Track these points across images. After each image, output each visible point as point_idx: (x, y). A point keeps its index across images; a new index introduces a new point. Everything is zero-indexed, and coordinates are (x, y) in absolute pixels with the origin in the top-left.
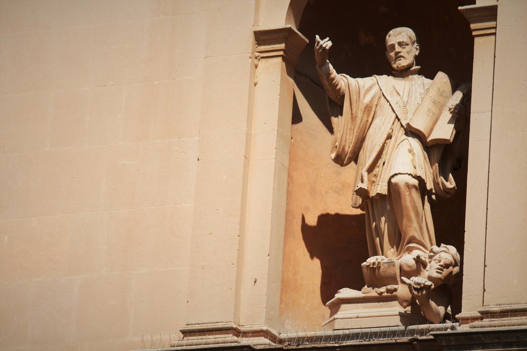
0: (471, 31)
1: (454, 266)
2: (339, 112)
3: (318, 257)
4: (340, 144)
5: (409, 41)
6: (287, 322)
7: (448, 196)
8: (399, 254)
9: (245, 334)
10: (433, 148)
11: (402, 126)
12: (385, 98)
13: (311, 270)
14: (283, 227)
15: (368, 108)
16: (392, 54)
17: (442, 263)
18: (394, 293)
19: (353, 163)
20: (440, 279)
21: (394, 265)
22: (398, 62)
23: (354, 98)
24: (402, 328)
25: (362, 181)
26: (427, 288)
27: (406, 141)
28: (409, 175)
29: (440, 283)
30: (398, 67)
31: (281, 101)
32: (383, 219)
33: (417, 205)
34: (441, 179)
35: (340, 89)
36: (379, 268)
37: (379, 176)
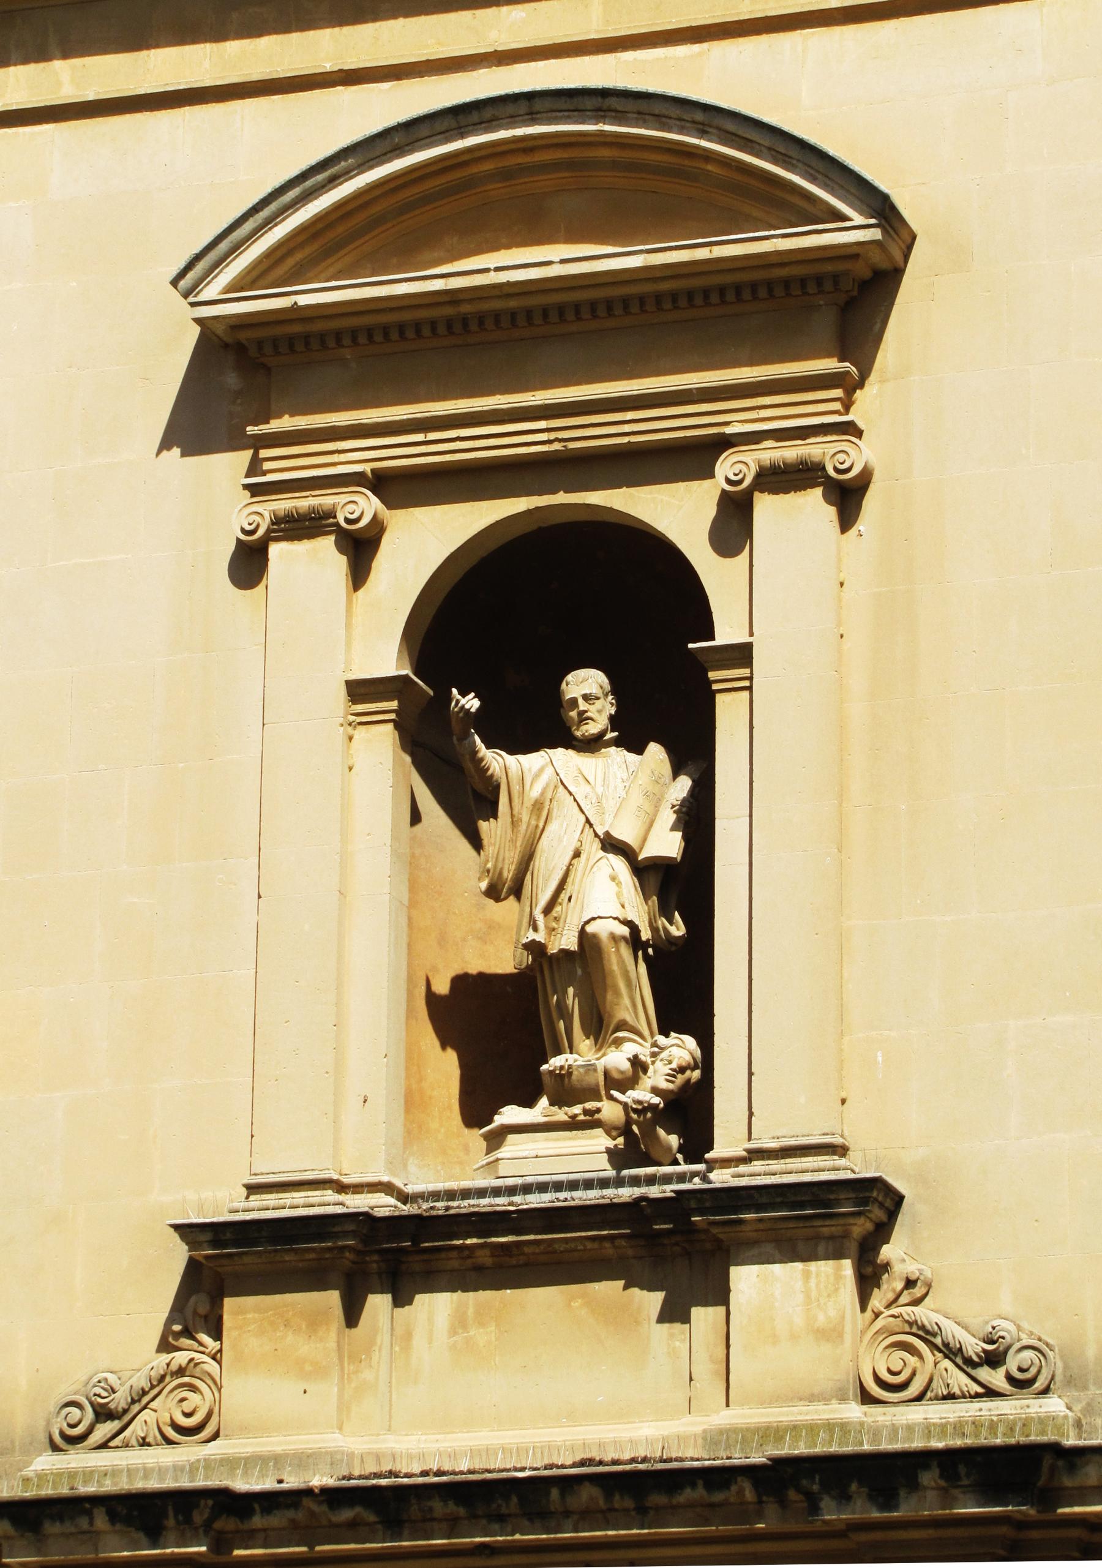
0: (710, 683)
1: (693, 1070)
2: (492, 812)
3: (454, 1047)
4: (495, 866)
5: (600, 693)
6: (411, 1161)
7: (673, 948)
8: (599, 1050)
9: (357, 1188)
10: (651, 874)
11: (596, 835)
12: (566, 788)
13: (445, 1069)
14: (404, 1006)
15: (538, 806)
16: (573, 714)
17: (674, 1065)
18: (597, 1116)
19: (512, 897)
20: (672, 1091)
21: (595, 1070)
22: (584, 728)
23: (516, 788)
24: (611, 1173)
25: (535, 929)
26: (653, 1107)
27: (604, 861)
28: (615, 919)
29: (672, 1097)
30: (583, 735)
31: (395, 795)
32: (571, 991)
33: (629, 968)
34: (662, 922)
35: (492, 776)
36: (570, 1074)
37: (562, 921)
